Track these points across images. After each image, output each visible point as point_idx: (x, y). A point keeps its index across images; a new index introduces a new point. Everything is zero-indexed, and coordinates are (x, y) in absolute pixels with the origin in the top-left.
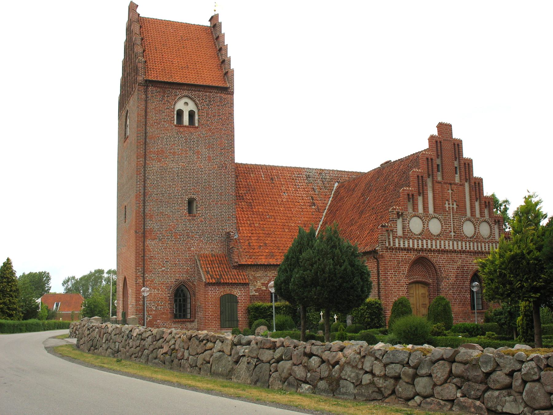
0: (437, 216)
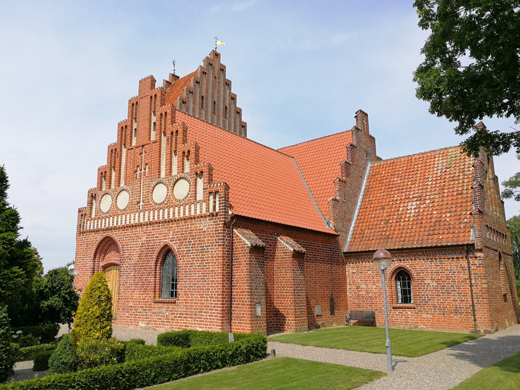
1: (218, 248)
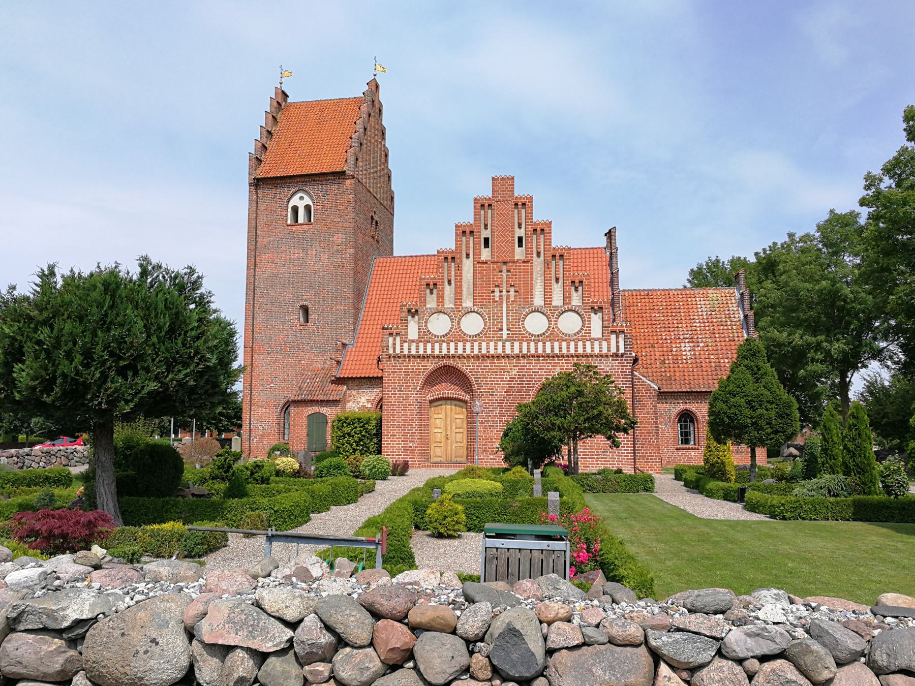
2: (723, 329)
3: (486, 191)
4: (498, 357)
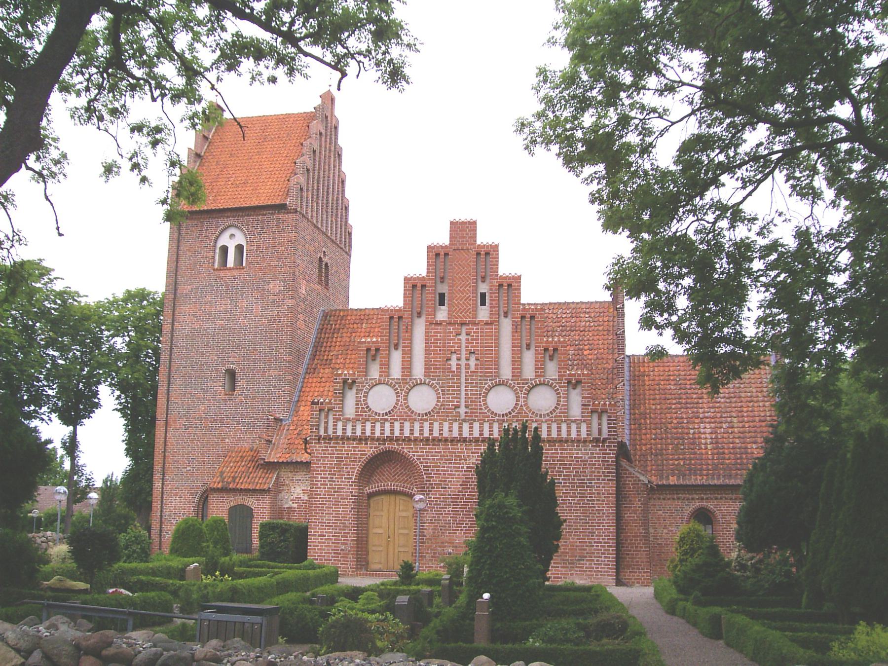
0: (428, 380)
1: (609, 484)
2: (753, 406)
3: (443, 238)
4: (452, 441)
